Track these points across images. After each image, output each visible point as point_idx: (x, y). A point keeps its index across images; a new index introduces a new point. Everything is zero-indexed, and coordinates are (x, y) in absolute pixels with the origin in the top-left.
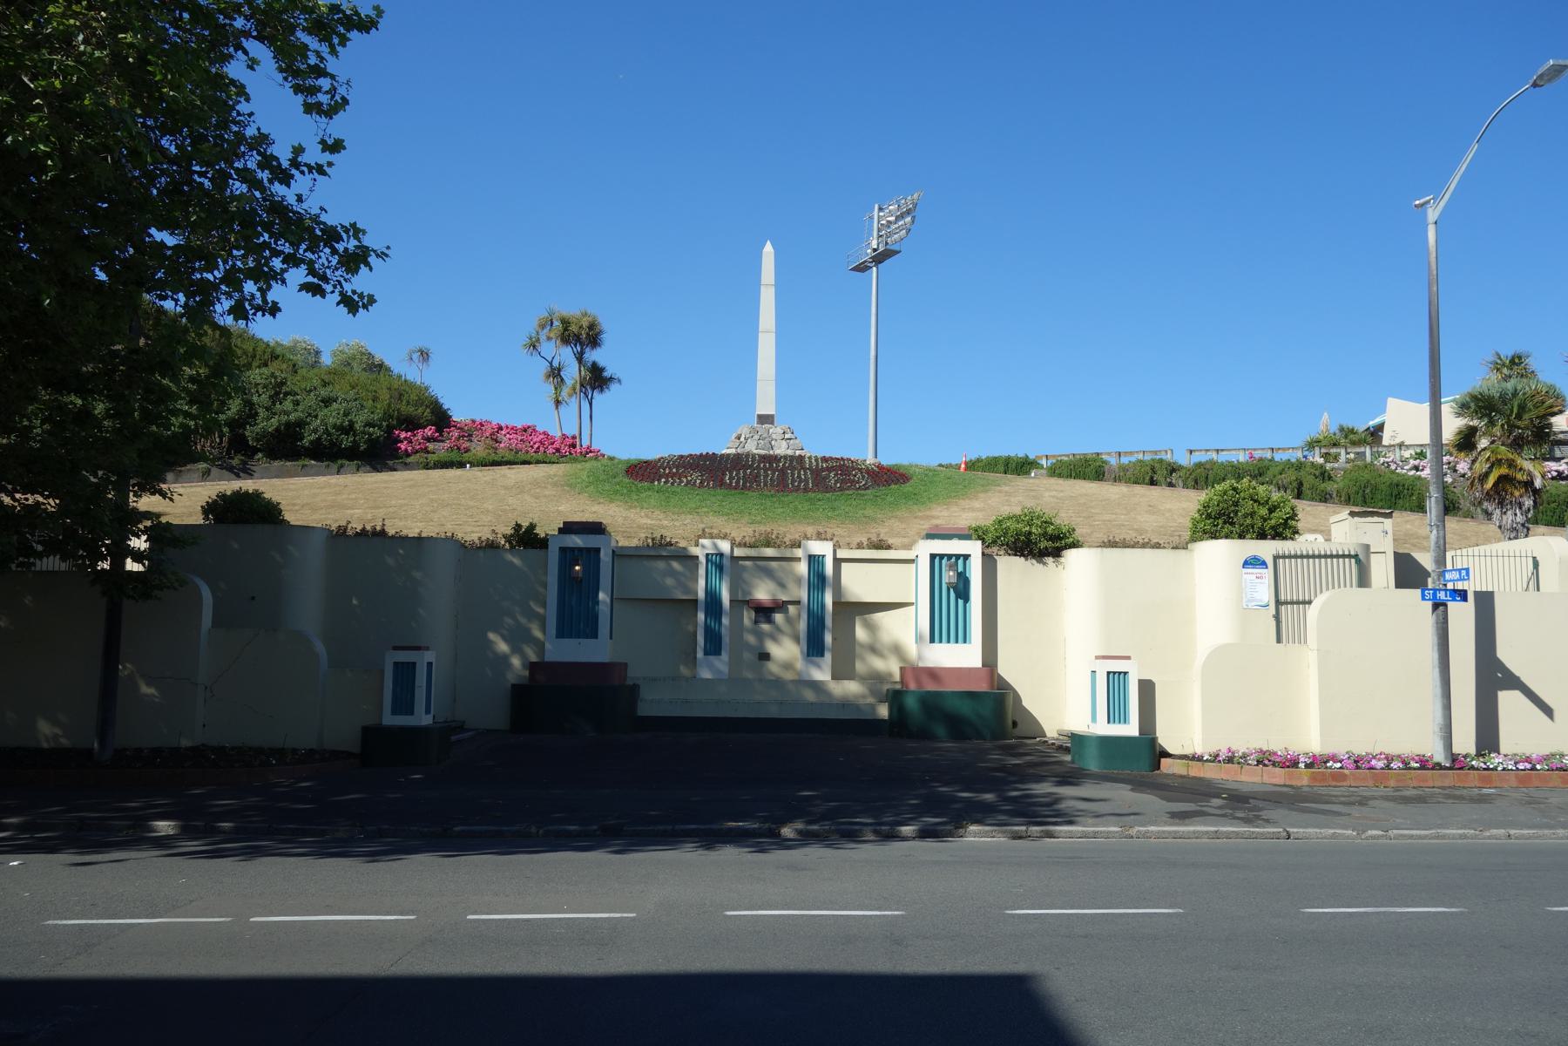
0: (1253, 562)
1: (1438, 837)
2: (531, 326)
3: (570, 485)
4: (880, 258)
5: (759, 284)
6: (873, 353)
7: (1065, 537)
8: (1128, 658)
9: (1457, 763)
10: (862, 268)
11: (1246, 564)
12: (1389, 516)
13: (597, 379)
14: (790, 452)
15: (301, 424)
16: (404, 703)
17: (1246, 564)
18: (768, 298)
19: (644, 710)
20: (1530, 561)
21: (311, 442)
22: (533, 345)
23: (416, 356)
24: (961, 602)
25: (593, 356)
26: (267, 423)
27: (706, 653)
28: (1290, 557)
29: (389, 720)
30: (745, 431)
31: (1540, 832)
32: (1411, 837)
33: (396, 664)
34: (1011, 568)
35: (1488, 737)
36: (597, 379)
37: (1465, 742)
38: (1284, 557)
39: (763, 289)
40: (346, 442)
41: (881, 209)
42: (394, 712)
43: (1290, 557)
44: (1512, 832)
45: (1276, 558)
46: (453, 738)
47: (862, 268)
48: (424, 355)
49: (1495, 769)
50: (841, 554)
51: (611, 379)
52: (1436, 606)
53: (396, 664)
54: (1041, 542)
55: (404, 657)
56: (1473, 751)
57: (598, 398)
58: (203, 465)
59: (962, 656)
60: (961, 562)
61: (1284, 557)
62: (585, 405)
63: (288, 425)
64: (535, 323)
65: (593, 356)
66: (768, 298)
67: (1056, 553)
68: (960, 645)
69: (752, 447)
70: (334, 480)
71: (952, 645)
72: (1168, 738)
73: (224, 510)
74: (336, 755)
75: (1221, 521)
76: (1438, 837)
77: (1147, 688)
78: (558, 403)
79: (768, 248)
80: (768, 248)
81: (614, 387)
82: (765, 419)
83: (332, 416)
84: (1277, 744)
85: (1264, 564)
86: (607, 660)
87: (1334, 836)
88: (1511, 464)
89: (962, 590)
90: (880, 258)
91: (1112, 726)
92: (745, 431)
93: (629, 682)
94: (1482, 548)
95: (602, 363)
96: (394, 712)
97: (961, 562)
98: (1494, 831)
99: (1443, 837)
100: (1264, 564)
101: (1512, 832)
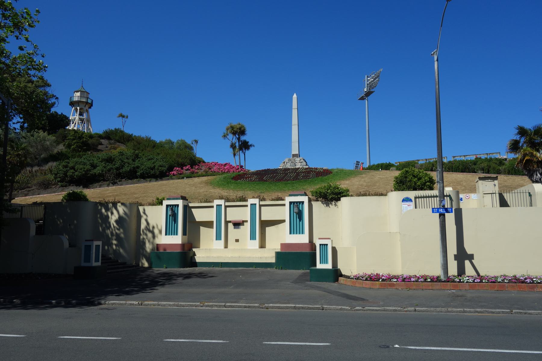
0: (406, 200)
1: (384, 310)
3: (207, 183)
4: (368, 94)
5: (292, 109)
6: (367, 129)
7: (343, 193)
9: (449, 280)
10: (362, 99)
11: (404, 200)
12: (496, 178)
13: (245, 146)
14: (301, 167)
15: (138, 167)
16: (88, 258)
17: (404, 200)
18: (295, 113)
19: (473, 261)
20: (528, 194)
21: (141, 173)
22: (225, 136)
23: (194, 142)
24: (298, 220)
25: (243, 138)
26: (126, 168)
28: (421, 197)
29: (83, 264)
30: (286, 160)
31: (429, 309)
32: (373, 310)
33: (86, 246)
34: (318, 206)
35: (461, 271)
36: (245, 146)
37: (453, 270)
38: (419, 197)
40: (152, 172)
41: (368, 77)
42: (85, 262)
43: (421, 197)
44: (417, 309)
45: (416, 198)
47: (362, 99)
48: (196, 142)
49: (463, 282)
50: (262, 203)
51: (251, 145)
52: (440, 215)
53: (86, 246)
54: (332, 196)
55: (88, 243)
56: (456, 274)
57: (247, 152)
58: (108, 182)
59: (303, 239)
60: (301, 205)
61: (419, 197)
63: (134, 168)
64: (225, 129)
65: (243, 138)
66: (295, 113)
67: (338, 199)
68: (301, 235)
69: (288, 166)
70: (146, 184)
71: (298, 235)
72: (345, 268)
75: (401, 184)
76: (384, 310)
77: (334, 250)
78: (235, 155)
79: (295, 96)
80: (295, 96)
81: (252, 149)
82: (294, 156)
83: (149, 164)
84: (383, 271)
85: (411, 200)
87: (341, 309)
88: (532, 155)
89: (300, 215)
90: (368, 94)
91: (321, 265)
92: (286, 160)
94: (519, 190)
95: (247, 140)
96: (85, 262)
97: (301, 205)
98: (409, 309)
99: (387, 310)
100: (411, 200)
101: (450, 309)
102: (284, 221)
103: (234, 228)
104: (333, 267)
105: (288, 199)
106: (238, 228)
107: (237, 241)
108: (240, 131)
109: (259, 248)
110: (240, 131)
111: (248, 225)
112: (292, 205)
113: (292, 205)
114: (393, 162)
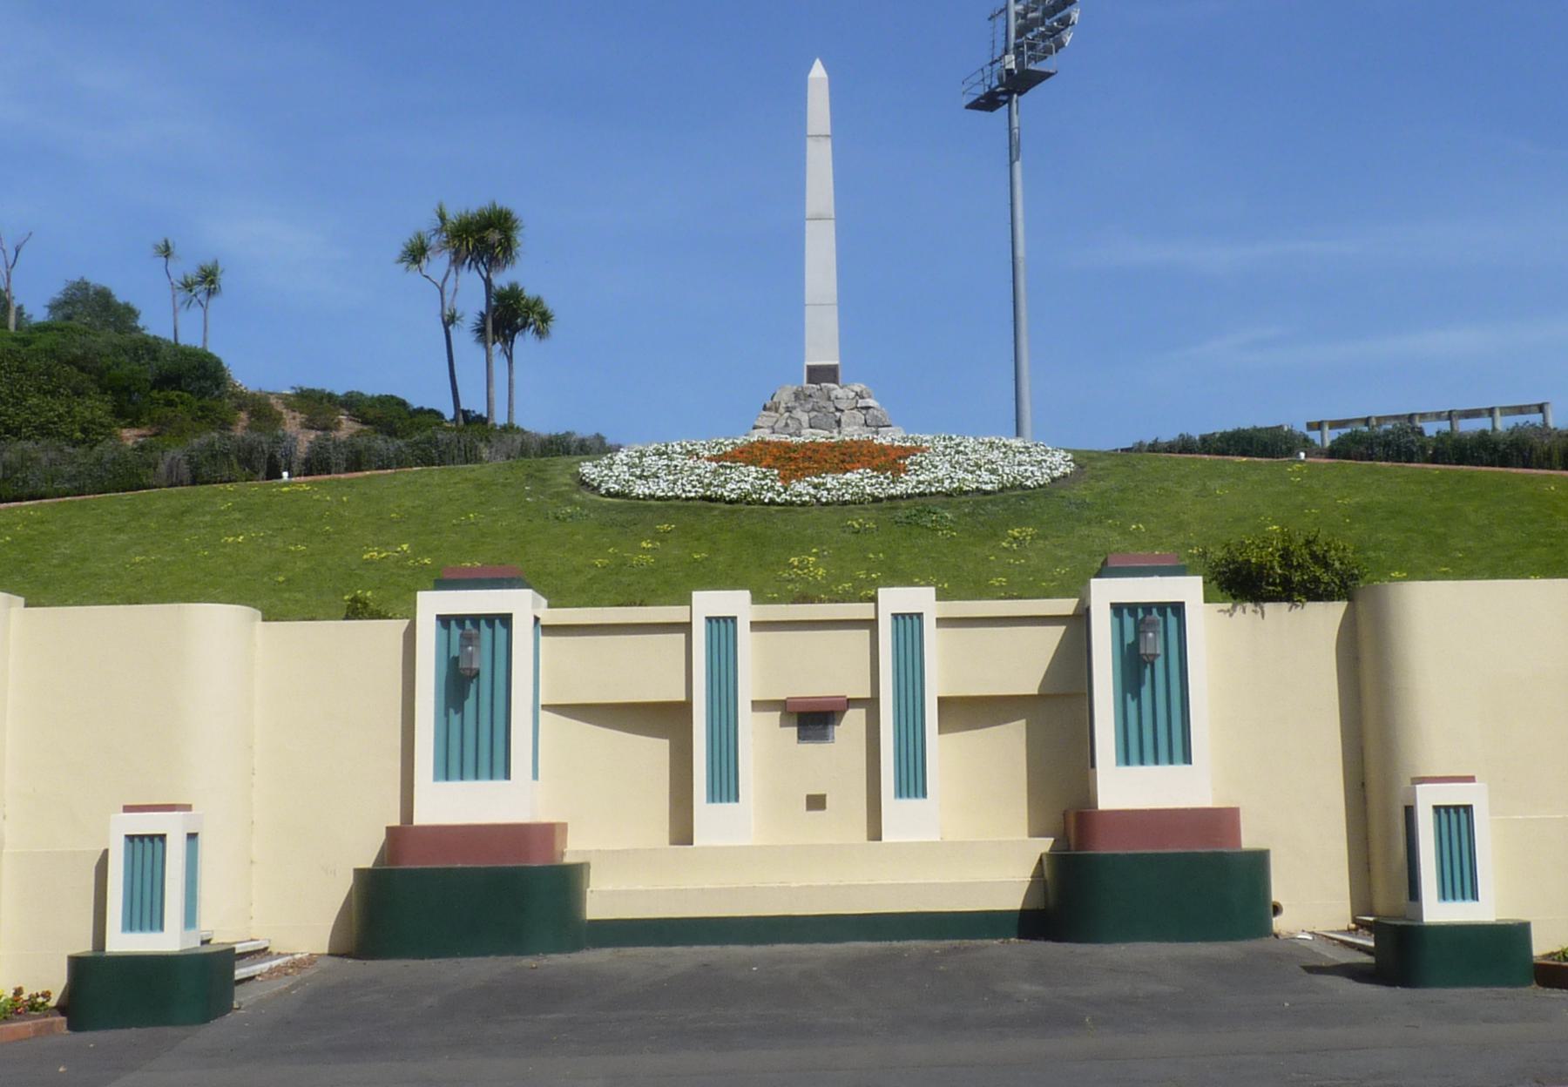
2: (424, 222)
8: (1471, 779)
13: (508, 317)
16: (144, 911)
18: (820, 161)
19: (598, 905)
22: (416, 253)
27: (900, 793)
29: (121, 942)
36: (508, 317)
39: (810, 143)
42: (130, 925)
46: (240, 973)
55: (1453, 795)
62: (499, 363)
66: (820, 161)
73: (879, 426)
74: (34, 1006)
79: (818, 72)
80: (818, 72)
82: (821, 374)
86: (1209, 804)
93: (568, 859)
96: (130, 925)
102: (758, 705)
103: (802, 737)
104: (95, 950)
105: (432, 604)
106: (823, 737)
107: (816, 802)
108: (484, 238)
109: (673, 843)
110: (484, 238)
111: (855, 719)
112: (901, 621)
113: (1129, 622)
114: (1295, 421)
